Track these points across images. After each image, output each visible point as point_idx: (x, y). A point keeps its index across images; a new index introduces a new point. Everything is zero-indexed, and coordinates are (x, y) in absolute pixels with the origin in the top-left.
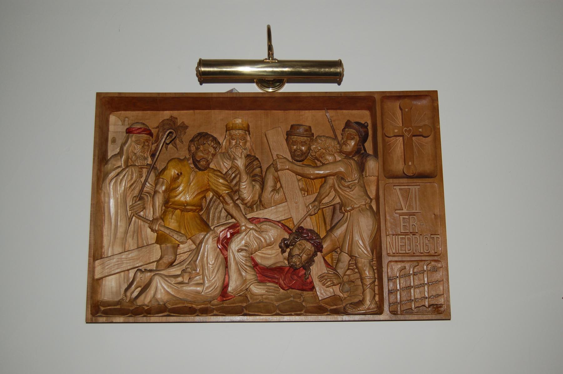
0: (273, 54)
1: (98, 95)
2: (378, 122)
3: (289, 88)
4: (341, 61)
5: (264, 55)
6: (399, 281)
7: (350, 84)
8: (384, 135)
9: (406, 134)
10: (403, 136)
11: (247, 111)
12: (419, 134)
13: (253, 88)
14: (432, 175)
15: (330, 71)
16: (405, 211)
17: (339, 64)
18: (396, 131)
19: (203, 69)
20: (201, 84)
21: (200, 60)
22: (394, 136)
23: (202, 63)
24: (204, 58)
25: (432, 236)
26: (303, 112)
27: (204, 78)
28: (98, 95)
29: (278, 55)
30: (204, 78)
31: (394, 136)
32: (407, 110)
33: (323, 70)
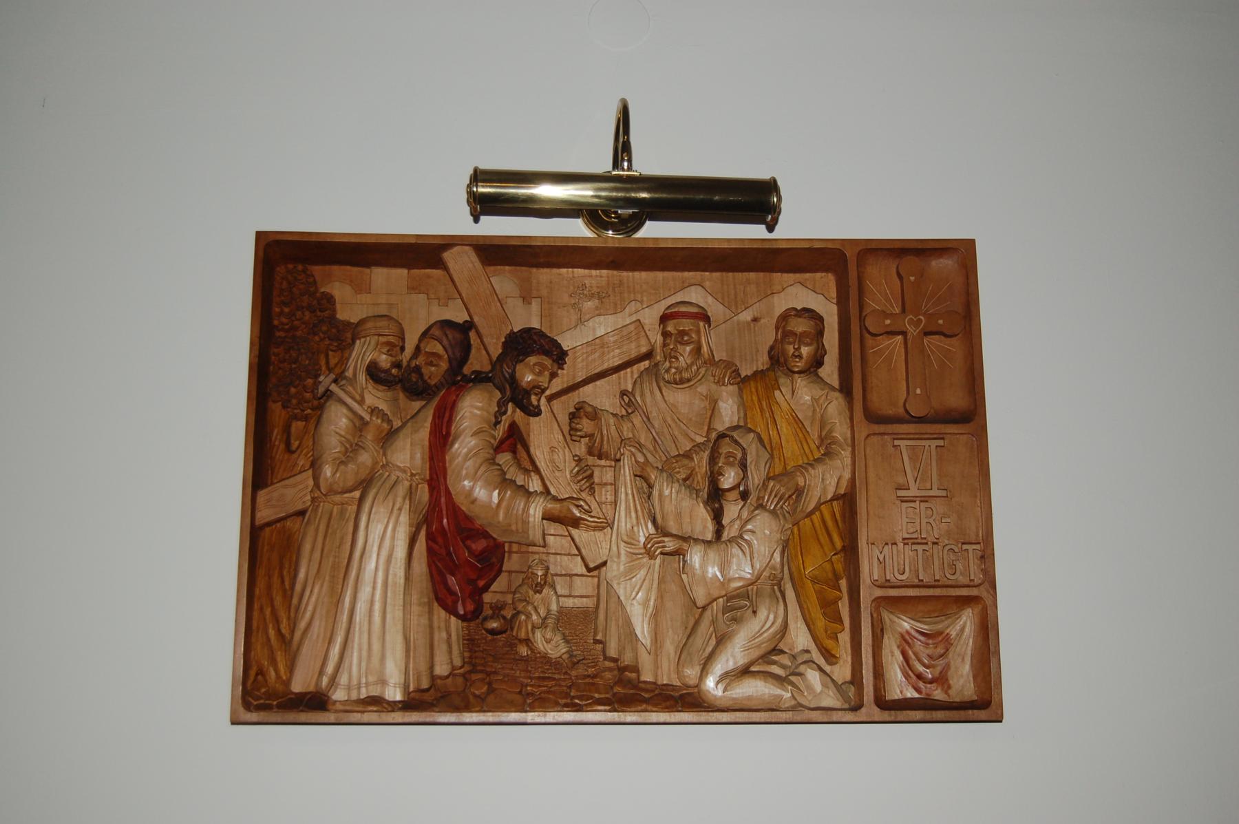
0: (630, 161)
1: (259, 235)
2: (852, 318)
3: (654, 230)
4: (775, 181)
5: (603, 164)
6: (910, 636)
7: (796, 224)
8: (863, 328)
9: (910, 329)
10: (904, 333)
11: (660, 275)
12: (934, 329)
13: (577, 229)
14: (969, 416)
15: (756, 200)
16: (913, 492)
17: (770, 187)
18: (888, 322)
19: (483, 189)
20: (476, 220)
21: (476, 170)
22: (903, 322)
23: (479, 176)
24: (486, 165)
25: (965, 547)
26: (785, 275)
27: (482, 206)
28: (259, 235)
29: (646, 162)
30: (482, 206)
31: (903, 322)
32: (912, 278)
33: (664, 196)
